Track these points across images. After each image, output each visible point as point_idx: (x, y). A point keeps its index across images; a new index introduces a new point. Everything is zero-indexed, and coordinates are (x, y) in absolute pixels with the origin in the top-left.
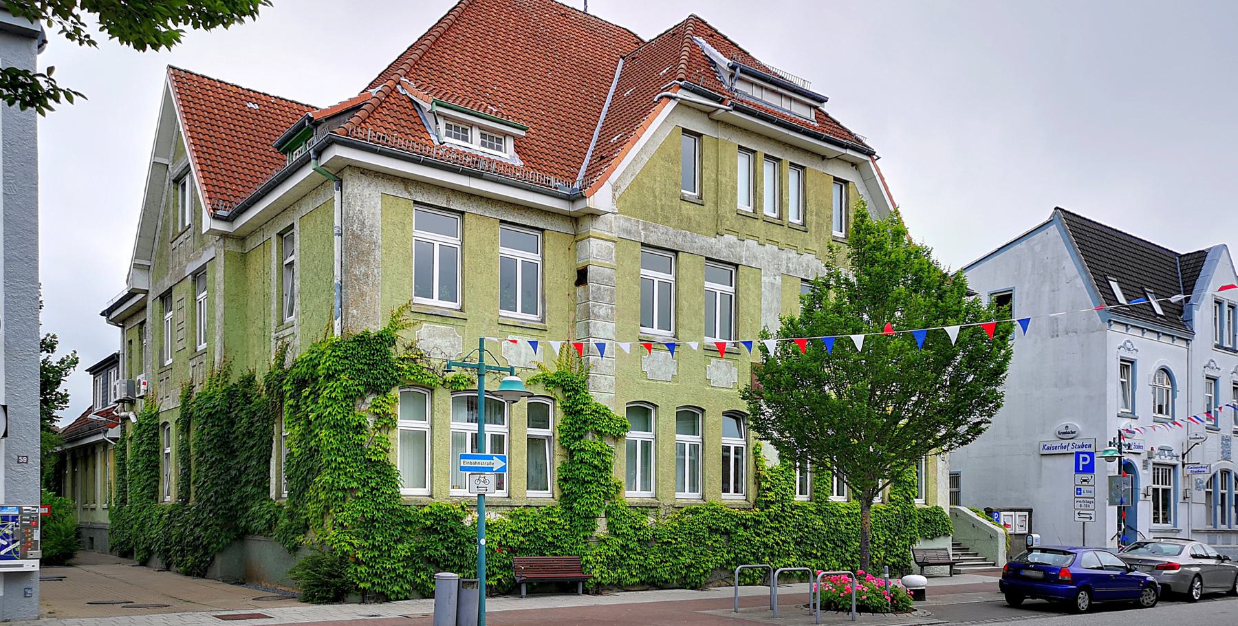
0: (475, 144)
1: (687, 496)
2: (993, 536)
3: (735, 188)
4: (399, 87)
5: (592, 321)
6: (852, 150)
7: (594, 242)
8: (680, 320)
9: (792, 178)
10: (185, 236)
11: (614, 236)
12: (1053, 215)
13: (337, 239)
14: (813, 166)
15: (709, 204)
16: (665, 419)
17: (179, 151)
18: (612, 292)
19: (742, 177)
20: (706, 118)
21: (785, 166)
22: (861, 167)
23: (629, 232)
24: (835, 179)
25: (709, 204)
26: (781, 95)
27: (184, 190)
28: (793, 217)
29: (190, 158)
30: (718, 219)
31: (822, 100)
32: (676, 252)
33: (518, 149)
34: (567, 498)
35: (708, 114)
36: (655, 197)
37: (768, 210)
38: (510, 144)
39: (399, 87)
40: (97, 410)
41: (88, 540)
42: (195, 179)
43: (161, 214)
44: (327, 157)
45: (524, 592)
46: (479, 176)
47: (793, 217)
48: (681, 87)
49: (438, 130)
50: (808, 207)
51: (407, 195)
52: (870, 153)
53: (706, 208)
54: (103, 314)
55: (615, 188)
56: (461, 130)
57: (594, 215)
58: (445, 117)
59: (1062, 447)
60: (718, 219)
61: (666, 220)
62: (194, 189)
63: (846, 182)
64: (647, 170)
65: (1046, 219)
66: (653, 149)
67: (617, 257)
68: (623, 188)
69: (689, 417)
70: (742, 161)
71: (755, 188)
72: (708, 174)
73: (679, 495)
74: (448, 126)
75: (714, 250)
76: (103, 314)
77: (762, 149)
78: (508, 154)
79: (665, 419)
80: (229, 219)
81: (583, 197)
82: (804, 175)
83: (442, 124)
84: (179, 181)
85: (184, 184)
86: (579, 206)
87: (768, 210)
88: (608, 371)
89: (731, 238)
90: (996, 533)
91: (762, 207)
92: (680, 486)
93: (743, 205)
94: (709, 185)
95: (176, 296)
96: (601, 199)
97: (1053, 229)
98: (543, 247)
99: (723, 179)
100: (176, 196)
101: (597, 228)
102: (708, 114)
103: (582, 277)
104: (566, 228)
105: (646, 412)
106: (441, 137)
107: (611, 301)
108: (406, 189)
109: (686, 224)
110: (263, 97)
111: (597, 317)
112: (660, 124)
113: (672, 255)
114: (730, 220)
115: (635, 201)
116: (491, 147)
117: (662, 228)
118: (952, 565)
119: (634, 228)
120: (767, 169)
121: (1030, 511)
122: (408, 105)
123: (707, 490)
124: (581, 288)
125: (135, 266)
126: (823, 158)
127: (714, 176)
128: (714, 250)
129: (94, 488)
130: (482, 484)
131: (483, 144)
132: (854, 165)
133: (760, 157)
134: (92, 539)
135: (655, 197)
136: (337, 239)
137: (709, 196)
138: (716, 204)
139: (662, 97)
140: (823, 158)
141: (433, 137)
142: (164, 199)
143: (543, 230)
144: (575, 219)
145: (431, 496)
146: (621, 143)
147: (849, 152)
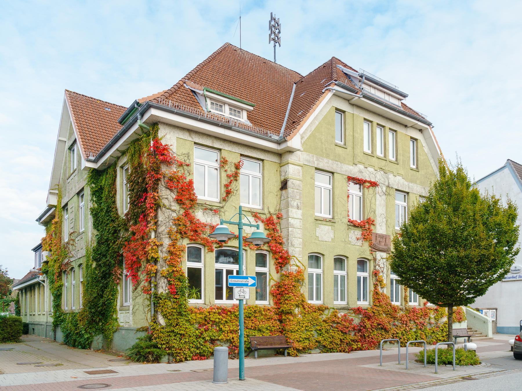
0: (226, 113)
1: (339, 303)
2: (485, 322)
3: (362, 140)
4: (185, 85)
5: (290, 209)
6: (418, 122)
7: (290, 166)
8: (336, 209)
9: (390, 136)
10: (74, 174)
11: (301, 163)
12: (506, 163)
13: (152, 145)
14: (401, 130)
15: (350, 148)
16: (328, 262)
17: (71, 133)
18: (300, 193)
19: (367, 136)
20: (347, 102)
21: (387, 130)
22: (424, 132)
23: (309, 162)
24: (411, 138)
25: (350, 148)
26: (384, 92)
27: (74, 153)
28: (391, 157)
29: (76, 135)
30: (354, 156)
31: (405, 96)
32: (333, 173)
33: (249, 118)
34: (277, 303)
35: (348, 100)
36: (322, 143)
37: (379, 152)
38: (245, 114)
39: (185, 85)
40: (36, 268)
41: (32, 330)
42: (79, 147)
43: (63, 166)
44: (146, 116)
45: (256, 356)
46: (229, 128)
47: (391, 157)
48: (336, 84)
49: (206, 105)
50: (399, 152)
51: (190, 139)
52: (429, 124)
53: (348, 150)
54: (37, 220)
55: (302, 138)
56: (220, 105)
57: (290, 151)
58: (211, 99)
59: (513, 277)
60: (354, 156)
61: (328, 156)
62: (78, 150)
63: (416, 140)
64: (317, 128)
65: (503, 165)
66: (321, 118)
67: (303, 175)
68: (306, 138)
69: (339, 261)
70: (365, 126)
71: (372, 141)
72: (349, 132)
73: (336, 303)
74: (212, 103)
75: (352, 172)
76: (37, 220)
77: (376, 120)
78: (243, 119)
79: (328, 262)
80: (95, 161)
81: (286, 141)
82: (396, 135)
83: (209, 102)
84: (71, 148)
85: (74, 150)
86: (283, 146)
87: (379, 152)
88: (299, 236)
89: (361, 167)
90: (487, 320)
91: (376, 151)
92: (336, 297)
93: (366, 149)
94: (349, 138)
95: (69, 206)
96: (295, 142)
97: (507, 171)
98: (263, 169)
99: (356, 135)
100: (70, 157)
101: (291, 158)
102: (348, 101)
103: (284, 185)
104: (275, 159)
105: (317, 259)
106: (208, 107)
107: (300, 198)
108: (190, 134)
109: (338, 159)
110: (113, 106)
111: (292, 207)
112: (325, 104)
113: (330, 175)
114: (360, 157)
115: (310, 146)
116: (235, 115)
117: (326, 160)
118: (469, 337)
119: (311, 159)
120: (378, 131)
121: (496, 309)
122: (191, 93)
123: (350, 300)
124: (284, 192)
125: (50, 193)
126: (406, 126)
127: (351, 133)
128: (352, 172)
129: (35, 305)
130: (242, 294)
131: (231, 114)
132: (421, 130)
133: (375, 125)
134: (33, 329)
135: (322, 143)
136: (152, 145)
137: (349, 144)
138: (353, 148)
139: (327, 90)
140: (406, 126)
141: (204, 109)
142: (64, 159)
143: (263, 160)
144: (280, 155)
145: (205, 304)
146: (304, 115)
147: (420, 123)
